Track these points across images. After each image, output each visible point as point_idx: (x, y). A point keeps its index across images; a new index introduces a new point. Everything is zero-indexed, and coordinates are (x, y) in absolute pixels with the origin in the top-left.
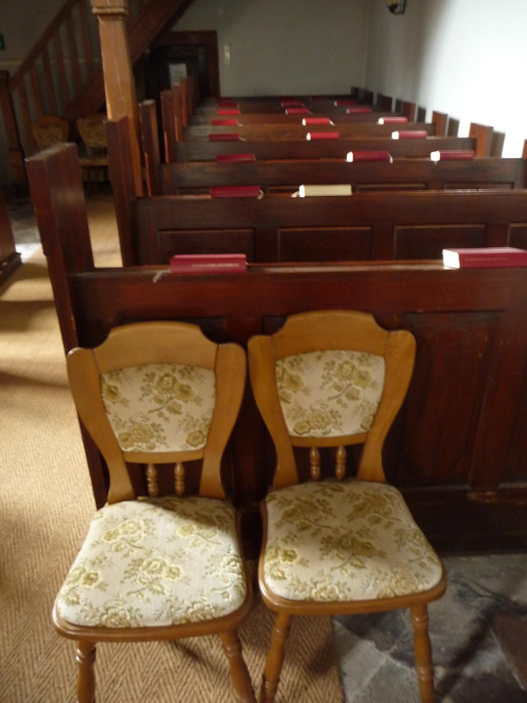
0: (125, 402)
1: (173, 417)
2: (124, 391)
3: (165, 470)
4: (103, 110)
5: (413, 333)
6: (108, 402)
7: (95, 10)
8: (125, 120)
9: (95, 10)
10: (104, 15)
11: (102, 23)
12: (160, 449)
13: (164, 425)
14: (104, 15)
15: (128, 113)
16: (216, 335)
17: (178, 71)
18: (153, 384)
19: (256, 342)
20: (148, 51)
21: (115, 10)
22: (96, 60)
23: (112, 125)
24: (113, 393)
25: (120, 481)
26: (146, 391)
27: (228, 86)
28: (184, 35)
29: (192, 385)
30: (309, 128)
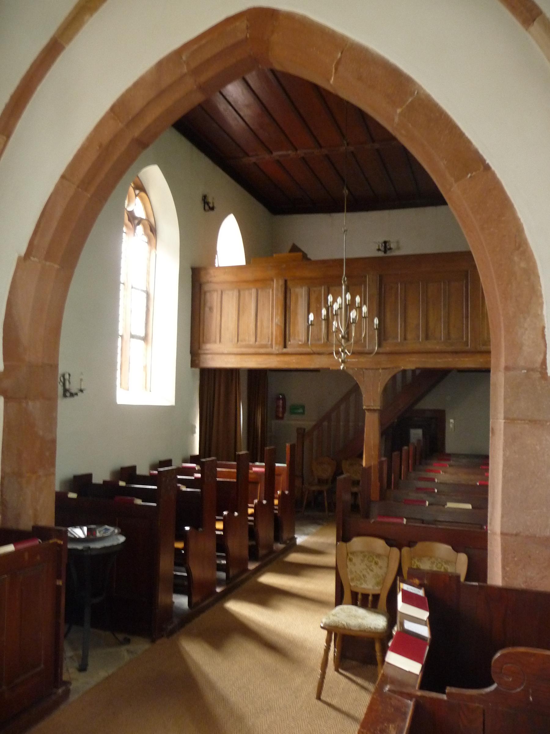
0: (355, 564)
1: (371, 573)
2: (355, 560)
3: (365, 596)
4: (361, 456)
5: (466, 554)
6: (349, 563)
7: (364, 407)
8: (370, 468)
9: (364, 407)
10: (369, 410)
11: (367, 414)
12: (364, 586)
13: (367, 575)
14: (369, 410)
15: (374, 462)
16: (390, 543)
17: (416, 434)
18: (366, 559)
19: (405, 550)
20: (396, 420)
21: (375, 408)
22: (360, 424)
23: (364, 469)
24: (351, 560)
25: (347, 595)
26: (362, 561)
27: (451, 446)
28: (424, 411)
29: (379, 561)
30: (271, 471)
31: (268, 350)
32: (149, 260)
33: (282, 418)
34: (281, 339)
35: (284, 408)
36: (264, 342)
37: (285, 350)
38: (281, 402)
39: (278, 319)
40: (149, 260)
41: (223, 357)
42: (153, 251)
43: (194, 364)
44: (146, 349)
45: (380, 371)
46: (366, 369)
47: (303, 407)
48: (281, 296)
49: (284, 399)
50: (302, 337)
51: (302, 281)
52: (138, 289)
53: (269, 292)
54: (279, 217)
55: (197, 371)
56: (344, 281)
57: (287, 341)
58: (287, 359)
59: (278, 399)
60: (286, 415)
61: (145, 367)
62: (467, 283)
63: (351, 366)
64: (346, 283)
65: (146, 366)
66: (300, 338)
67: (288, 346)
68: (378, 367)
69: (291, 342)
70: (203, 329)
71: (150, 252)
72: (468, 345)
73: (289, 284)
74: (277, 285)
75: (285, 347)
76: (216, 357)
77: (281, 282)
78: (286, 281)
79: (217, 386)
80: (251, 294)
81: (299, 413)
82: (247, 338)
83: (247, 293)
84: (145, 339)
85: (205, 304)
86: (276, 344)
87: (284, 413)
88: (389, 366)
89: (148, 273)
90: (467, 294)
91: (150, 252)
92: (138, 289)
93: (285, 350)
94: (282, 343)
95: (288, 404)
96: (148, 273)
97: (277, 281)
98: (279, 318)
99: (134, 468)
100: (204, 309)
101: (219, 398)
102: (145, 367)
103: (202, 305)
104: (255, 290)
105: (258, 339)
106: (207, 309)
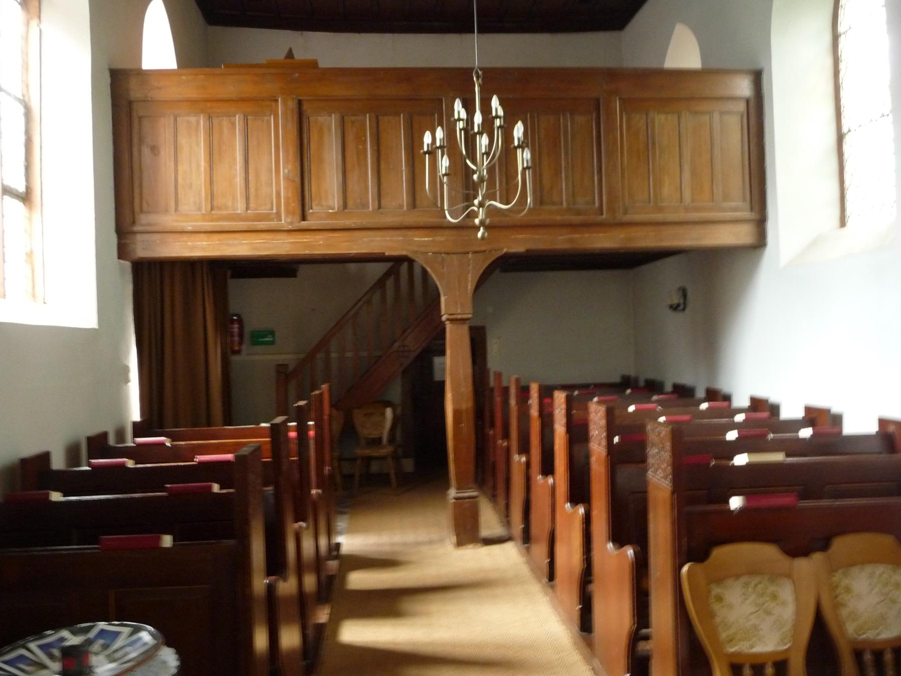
9: (444, 318)
21: (465, 316)
31: (273, 224)
32: (26, 39)
33: (238, 352)
34: (295, 205)
35: (241, 335)
36: (263, 210)
37: (304, 224)
38: (236, 326)
39: (287, 168)
40: (26, 39)
41: (185, 238)
42: (34, 23)
43: (123, 252)
44: (30, 219)
45: (470, 255)
46: (448, 254)
47: (272, 333)
48: (293, 128)
49: (240, 321)
50: (334, 201)
51: (328, 103)
52: (9, 94)
53: (269, 123)
54: (218, 29)
55: (127, 265)
56: (478, 77)
57: (307, 207)
58: (307, 238)
59: (233, 322)
60: (244, 347)
61: (30, 255)
62: (598, 118)
63: (422, 249)
64: (480, 80)
65: (31, 252)
66: (330, 203)
67: (309, 218)
68: (467, 250)
69: (315, 209)
70: (141, 186)
71: (28, 24)
72: (602, 214)
73: (305, 106)
74: (283, 108)
75: (304, 218)
76: (170, 238)
77: (292, 104)
78: (300, 103)
79: (167, 293)
80: (234, 124)
81: (267, 343)
82: (230, 204)
83: (225, 122)
84: (26, 198)
85: (141, 140)
86: (288, 212)
87: (241, 343)
88: (483, 248)
89: (26, 67)
90: (599, 132)
91: (28, 24)
92: (9, 94)
93: (304, 224)
94: (298, 211)
95: (248, 329)
96: (26, 67)
97: (285, 102)
98: (290, 166)
99: (45, 457)
100: (140, 151)
101: (173, 313)
102: (30, 255)
103: (135, 140)
104: (242, 117)
105: (252, 205)
106: (146, 151)
